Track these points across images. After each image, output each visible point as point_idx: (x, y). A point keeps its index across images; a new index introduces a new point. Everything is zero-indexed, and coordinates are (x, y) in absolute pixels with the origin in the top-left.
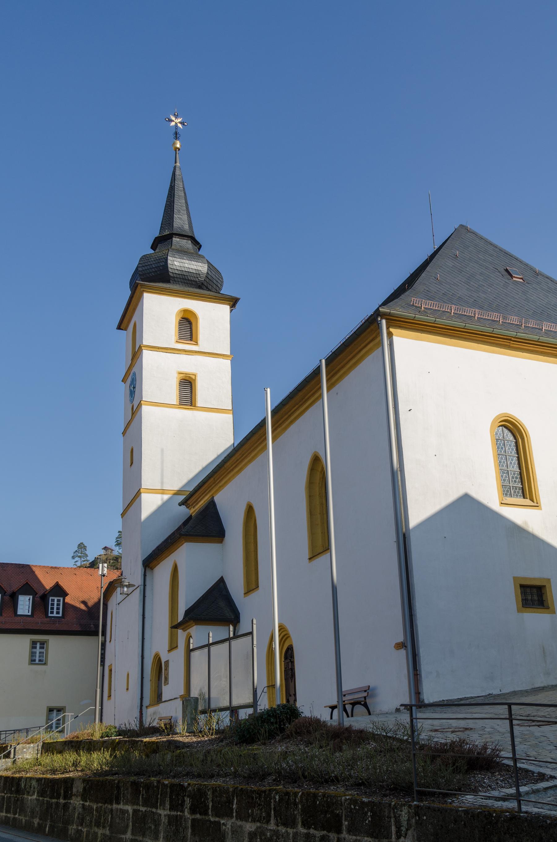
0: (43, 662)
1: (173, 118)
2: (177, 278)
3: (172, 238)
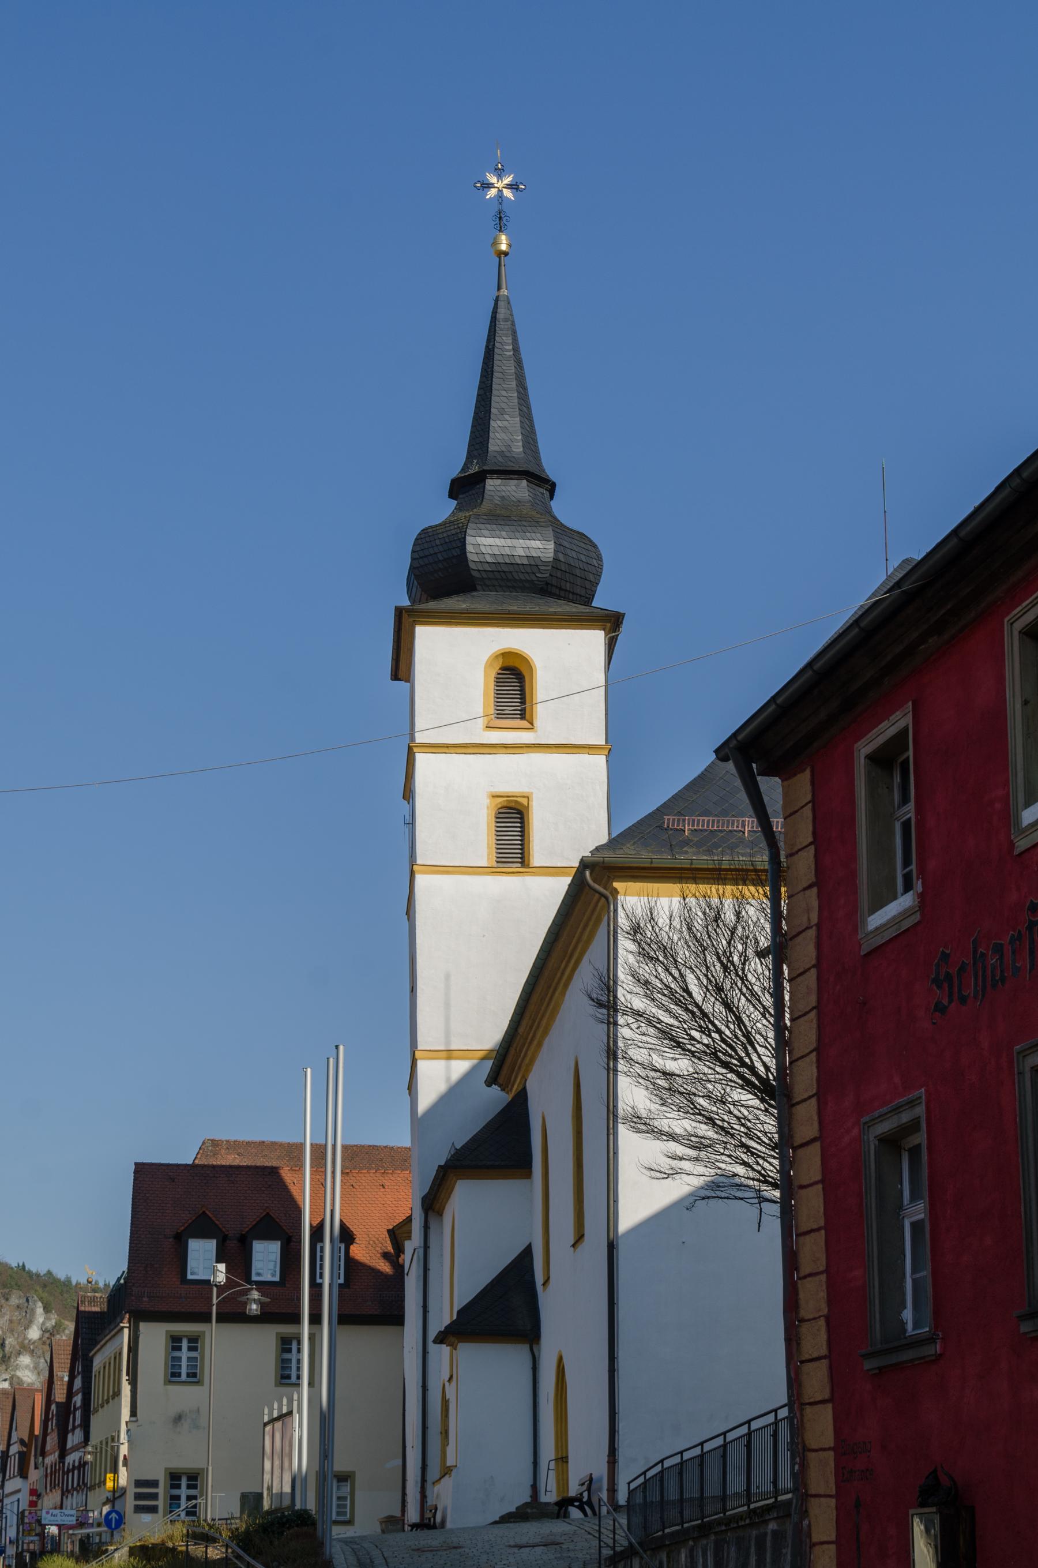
0: (194, 1377)
1: (493, 179)
2: (489, 579)
3: (483, 481)
